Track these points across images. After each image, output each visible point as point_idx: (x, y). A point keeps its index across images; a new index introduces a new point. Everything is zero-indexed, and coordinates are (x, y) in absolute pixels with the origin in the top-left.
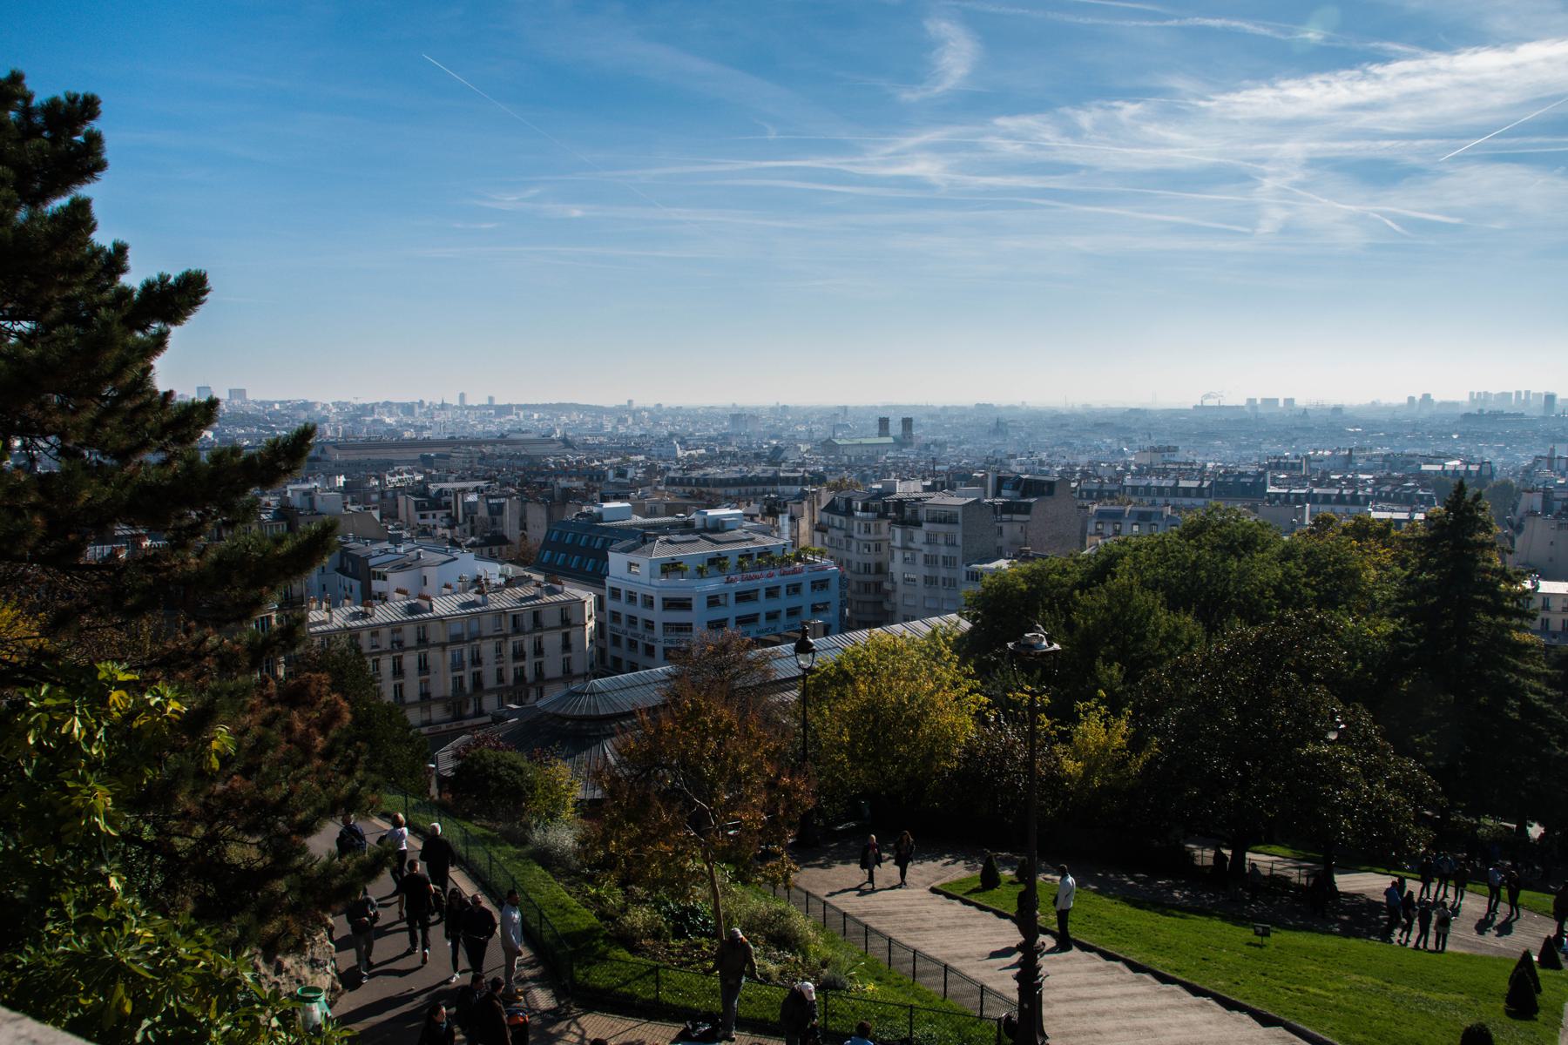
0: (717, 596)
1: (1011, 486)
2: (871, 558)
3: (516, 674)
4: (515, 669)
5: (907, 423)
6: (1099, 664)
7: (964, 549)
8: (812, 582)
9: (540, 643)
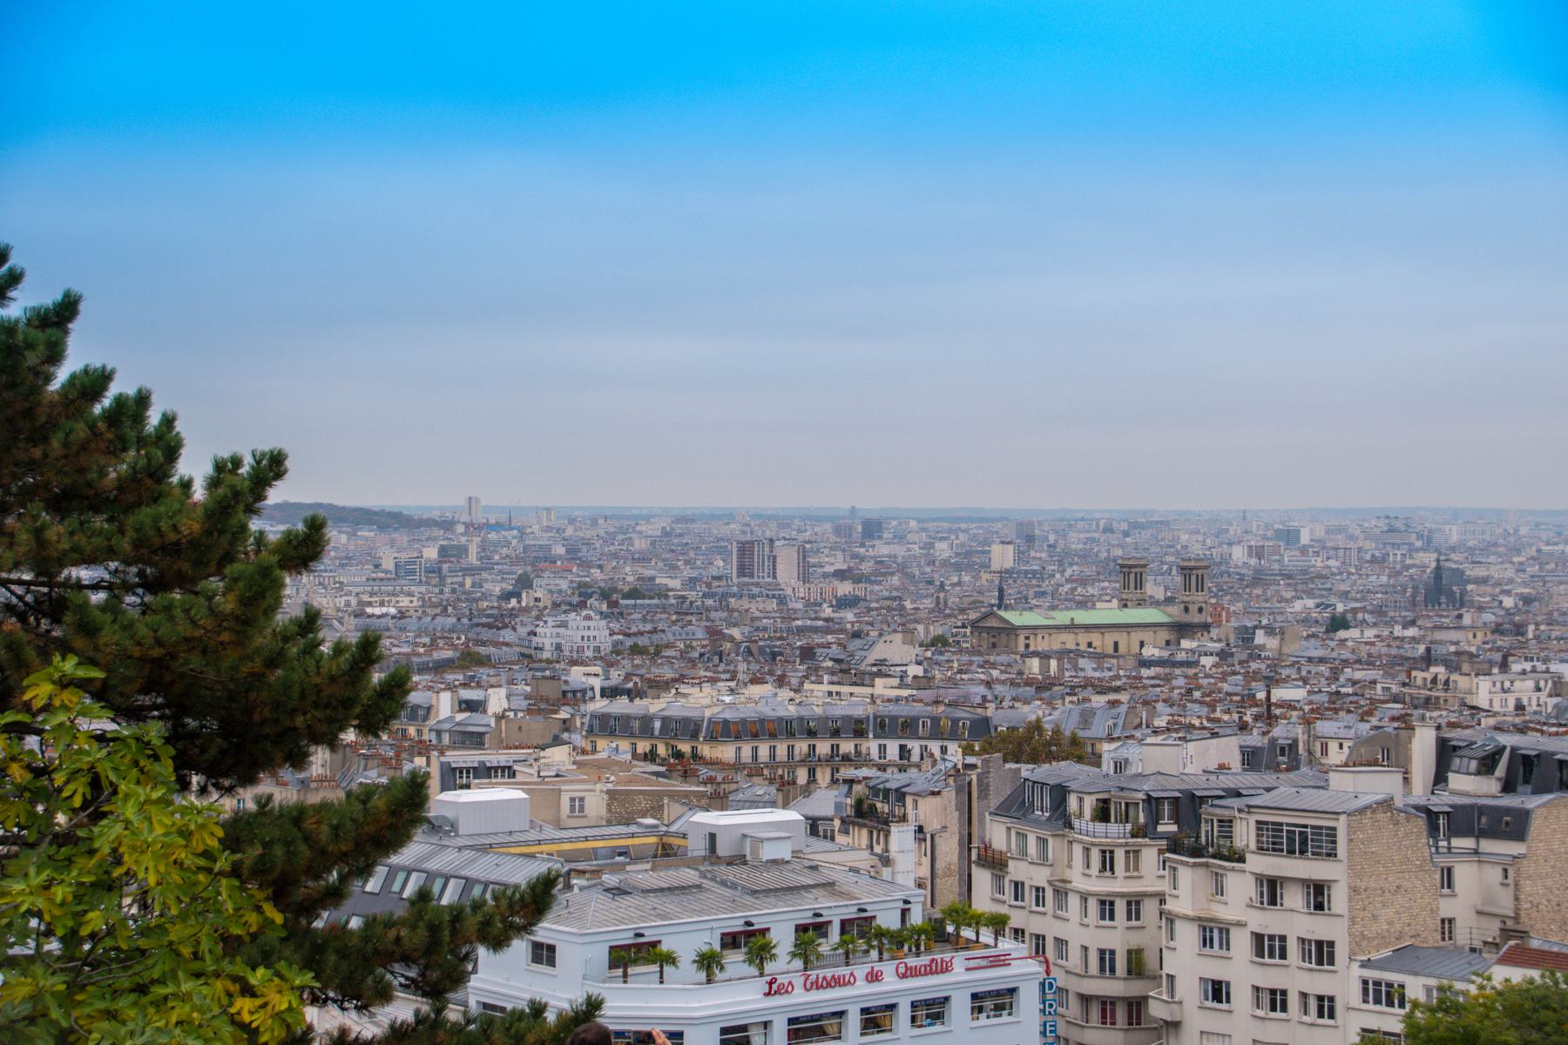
0: (744, 1028)
1: (1474, 765)
2: (1117, 937)
3: (1129, 961)
5: (1192, 574)
6: (1324, 761)
7: (1353, 921)
8: (975, 996)
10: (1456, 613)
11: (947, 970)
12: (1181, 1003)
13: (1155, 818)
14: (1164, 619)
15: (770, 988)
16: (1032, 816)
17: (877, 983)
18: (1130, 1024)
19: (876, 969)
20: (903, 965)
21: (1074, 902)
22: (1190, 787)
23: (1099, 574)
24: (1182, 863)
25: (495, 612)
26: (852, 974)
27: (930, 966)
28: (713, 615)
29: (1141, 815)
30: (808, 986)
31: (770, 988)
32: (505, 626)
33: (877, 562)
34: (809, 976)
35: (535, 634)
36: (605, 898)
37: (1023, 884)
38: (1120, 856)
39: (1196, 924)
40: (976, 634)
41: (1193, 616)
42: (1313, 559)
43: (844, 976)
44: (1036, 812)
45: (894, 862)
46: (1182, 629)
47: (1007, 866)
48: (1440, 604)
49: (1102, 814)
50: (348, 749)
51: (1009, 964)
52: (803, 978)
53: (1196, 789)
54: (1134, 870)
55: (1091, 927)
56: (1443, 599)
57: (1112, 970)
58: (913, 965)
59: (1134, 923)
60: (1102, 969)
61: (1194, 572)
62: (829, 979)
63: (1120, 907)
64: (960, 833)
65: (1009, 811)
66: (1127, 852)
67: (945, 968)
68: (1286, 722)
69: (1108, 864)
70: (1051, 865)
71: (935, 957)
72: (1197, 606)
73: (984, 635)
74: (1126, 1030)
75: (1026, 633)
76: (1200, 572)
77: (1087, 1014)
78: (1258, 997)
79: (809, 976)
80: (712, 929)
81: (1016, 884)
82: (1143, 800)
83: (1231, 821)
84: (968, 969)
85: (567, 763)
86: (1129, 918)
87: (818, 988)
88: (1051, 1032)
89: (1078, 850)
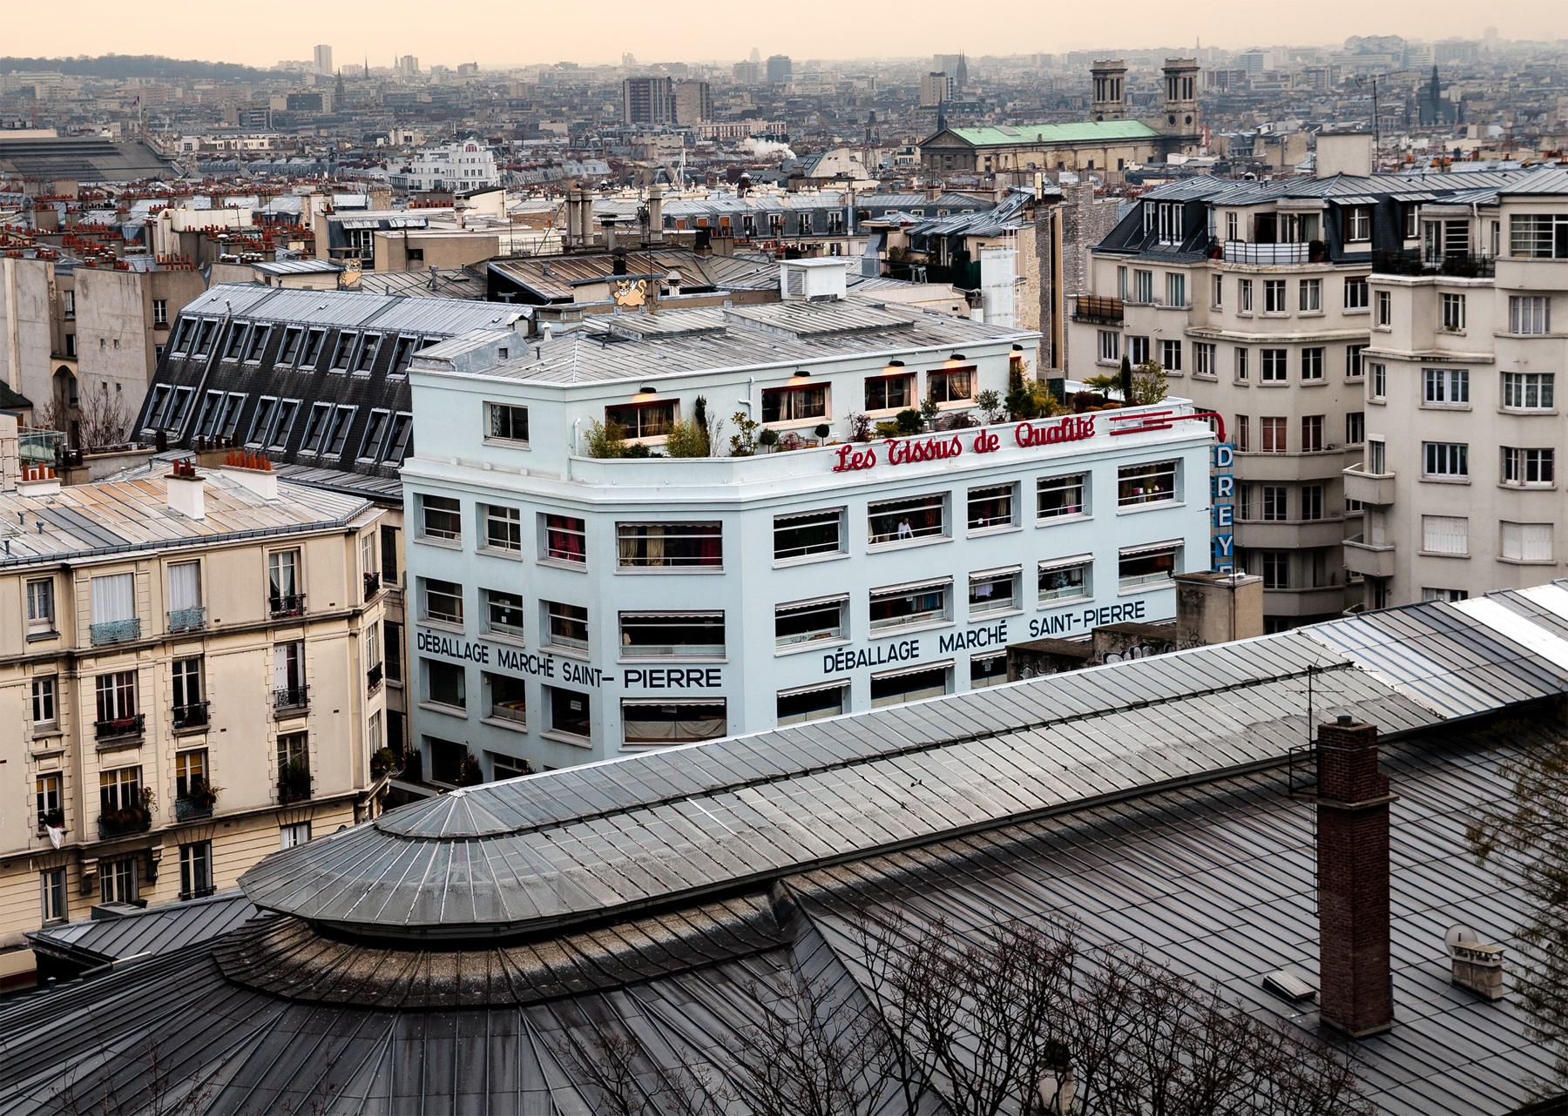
3: (107, 796)
4: (108, 775)
9: (193, 681)
10: (1460, 126)
11: (1086, 436)
12: (1392, 478)
13: (1343, 235)
14: (1146, 133)
15: (843, 460)
16: (1156, 248)
17: (989, 454)
18: (1306, 517)
19: (988, 434)
20: (1026, 428)
21: (1225, 358)
22: (1388, 191)
23: (1044, 107)
24: (1398, 285)
25: (360, 151)
26: (955, 441)
27: (1064, 428)
28: (615, 150)
29: (1322, 231)
30: (895, 458)
31: (843, 460)
32: (374, 165)
33: (788, 103)
34: (896, 443)
35: (410, 171)
36: (595, 348)
37: (1146, 340)
38: (1293, 289)
39: (1418, 368)
40: (928, 157)
41: (1180, 128)
42: (1282, 84)
43: (945, 443)
44: (1162, 243)
45: (986, 300)
46: (1165, 144)
47: (1121, 318)
48: (1436, 121)
49: (1265, 230)
50: (202, 237)
51: (1170, 426)
52: (888, 446)
53: (1397, 193)
54: (1313, 308)
55: (1253, 388)
56: (1440, 116)
57: (1282, 445)
58: (1039, 427)
59: (1312, 380)
60: (1267, 446)
61: (1182, 75)
62: (924, 447)
63: (1294, 360)
64: (1042, 288)
65: (1120, 245)
66: (1303, 283)
67: (1084, 433)
68: (1411, 166)
69: (1275, 295)
70: (1189, 310)
71: (1070, 416)
72: (1184, 116)
73: (937, 158)
74: (1300, 525)
75: (986, 153)
76: (1188, 75)
77: (1244, 502)
78: (1509, 463)
79: (896, 443)
80: (750, 383)
81: (1137, 340)
82: (1324, 210)
83: (1466, 223)
84: (1113, 434)
85: (500, 215)
86: (1306, 375)
87: (908, 460)
88: (1225, 519)
89: (1230, 286)
